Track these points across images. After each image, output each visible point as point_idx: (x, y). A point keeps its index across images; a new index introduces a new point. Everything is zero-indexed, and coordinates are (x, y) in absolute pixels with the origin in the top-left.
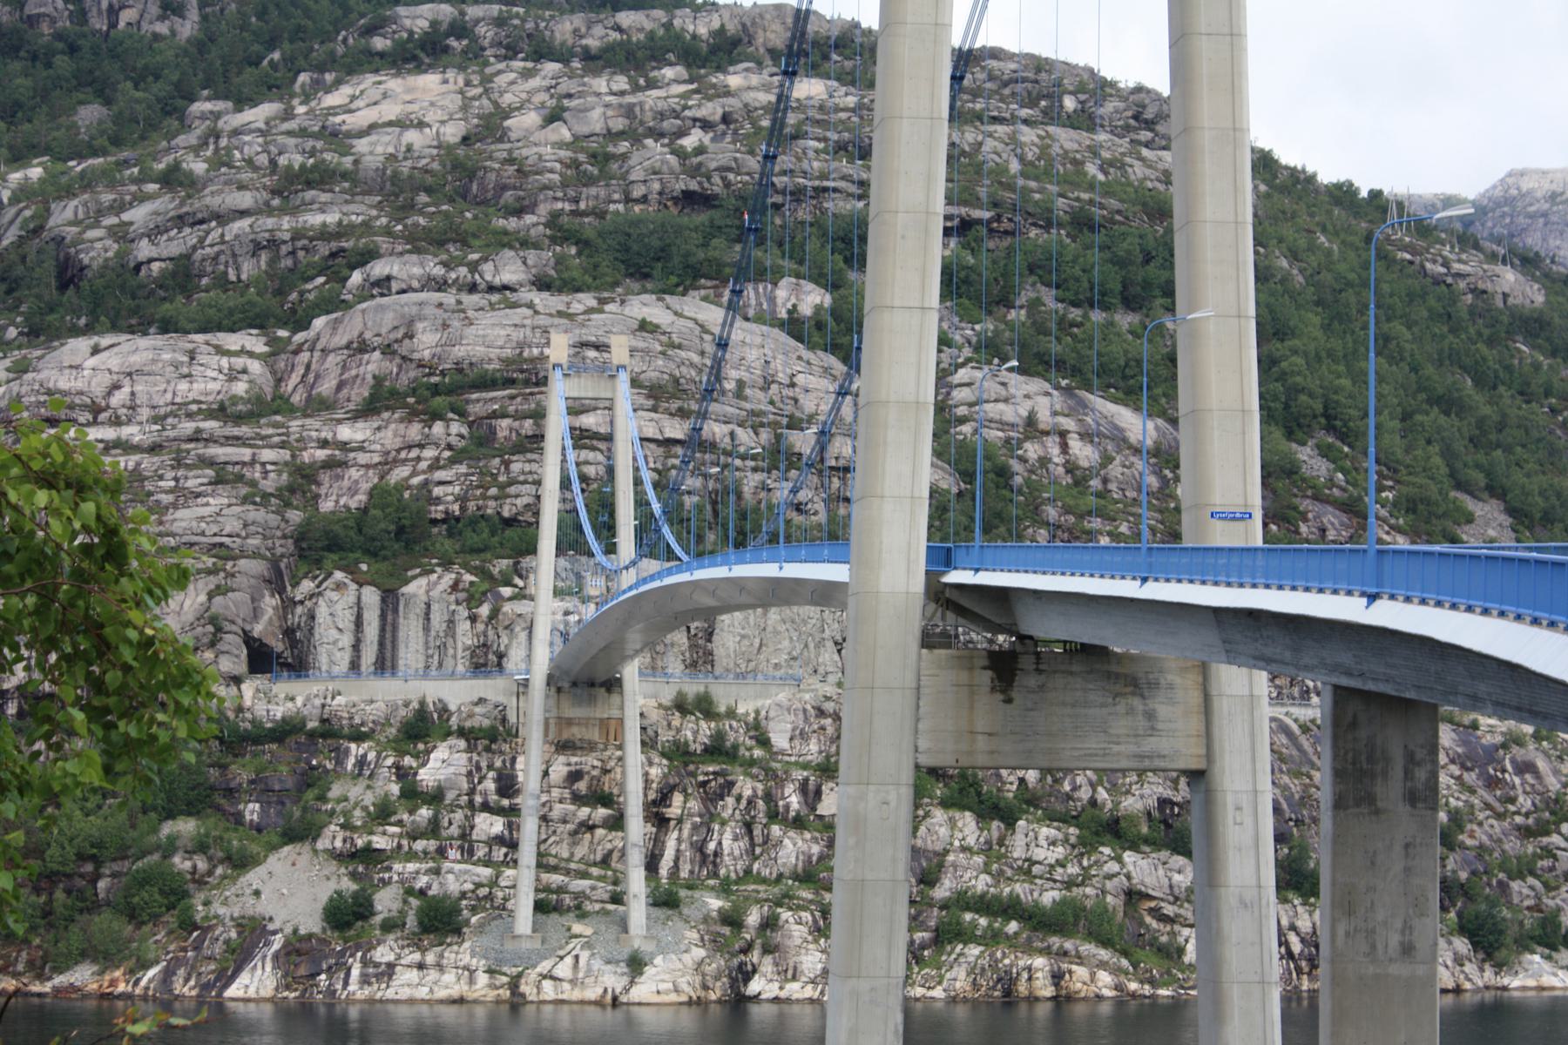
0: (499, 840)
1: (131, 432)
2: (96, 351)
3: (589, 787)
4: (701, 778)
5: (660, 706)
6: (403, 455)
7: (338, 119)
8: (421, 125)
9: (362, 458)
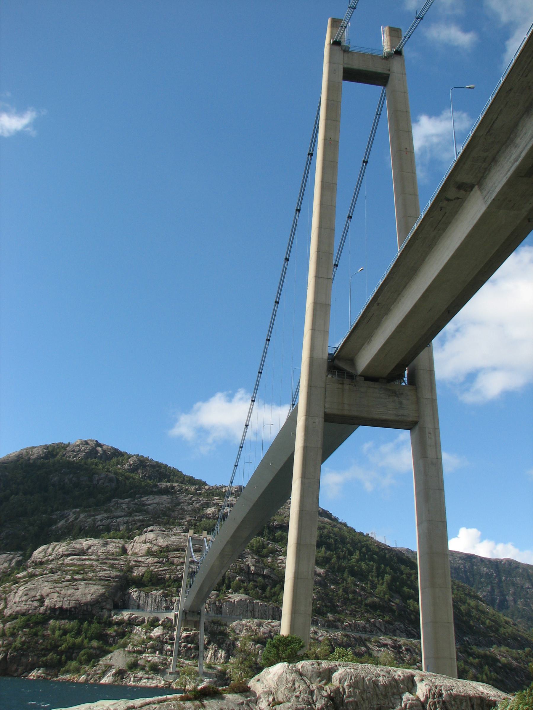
0: (169, 650)
1: (93, 557)
2: (86, 540)
3: (191, 640)
4: (218, 639)
5: (209, 622)
6: (153, 565)
7: (144, 502)
8: (162, 504)
9: (143, 565)
